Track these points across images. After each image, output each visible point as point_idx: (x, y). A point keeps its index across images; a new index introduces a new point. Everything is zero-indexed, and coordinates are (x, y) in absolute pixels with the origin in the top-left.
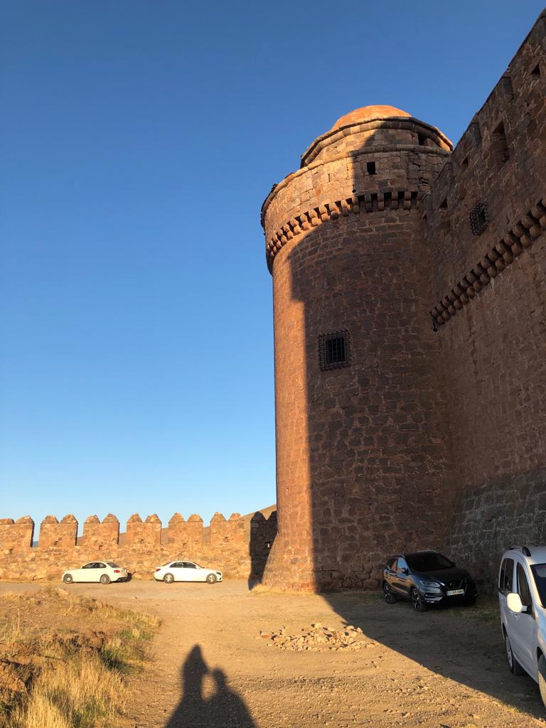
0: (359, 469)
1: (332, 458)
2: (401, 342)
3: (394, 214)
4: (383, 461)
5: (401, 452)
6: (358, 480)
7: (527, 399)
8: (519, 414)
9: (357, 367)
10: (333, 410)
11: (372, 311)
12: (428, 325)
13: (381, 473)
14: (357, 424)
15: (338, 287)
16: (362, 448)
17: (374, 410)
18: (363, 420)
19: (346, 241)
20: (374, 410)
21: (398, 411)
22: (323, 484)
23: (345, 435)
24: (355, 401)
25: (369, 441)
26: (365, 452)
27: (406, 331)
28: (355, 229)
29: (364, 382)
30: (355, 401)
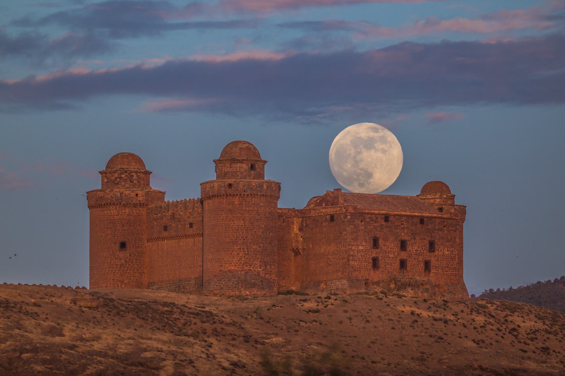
0: (127, 276)
1: (120, 273)
2: (140, 246)
3: (141, 209)
4: (133, 275)
5: (138, 273)
6: (127, 279)
7: (169, 267)
8: (167, 270)
9: (129, 251)
10: (121, 261)
11: (134, 236)
12: (146, 241)
13: (133, 278)
14: (128, 265)
15: (125, 228)
16: (129, 271)
17: (132, 262)
18: (129, 265)
19: (128, 215)
20: (132, 262)
21: (138, 263)
22: (117, 279)
23: (124, 268)
24: (128, 260)
25: (130, 270)
26: (129, 273)
27: (141, 243)
28: (130, 212)
29: (130, 255)
30: (128, 260)
